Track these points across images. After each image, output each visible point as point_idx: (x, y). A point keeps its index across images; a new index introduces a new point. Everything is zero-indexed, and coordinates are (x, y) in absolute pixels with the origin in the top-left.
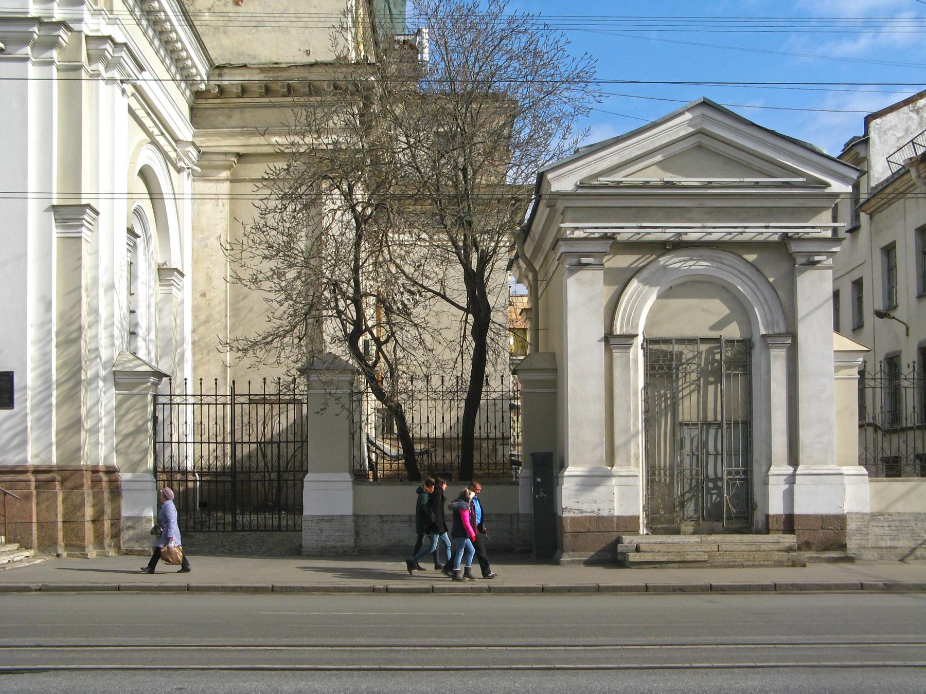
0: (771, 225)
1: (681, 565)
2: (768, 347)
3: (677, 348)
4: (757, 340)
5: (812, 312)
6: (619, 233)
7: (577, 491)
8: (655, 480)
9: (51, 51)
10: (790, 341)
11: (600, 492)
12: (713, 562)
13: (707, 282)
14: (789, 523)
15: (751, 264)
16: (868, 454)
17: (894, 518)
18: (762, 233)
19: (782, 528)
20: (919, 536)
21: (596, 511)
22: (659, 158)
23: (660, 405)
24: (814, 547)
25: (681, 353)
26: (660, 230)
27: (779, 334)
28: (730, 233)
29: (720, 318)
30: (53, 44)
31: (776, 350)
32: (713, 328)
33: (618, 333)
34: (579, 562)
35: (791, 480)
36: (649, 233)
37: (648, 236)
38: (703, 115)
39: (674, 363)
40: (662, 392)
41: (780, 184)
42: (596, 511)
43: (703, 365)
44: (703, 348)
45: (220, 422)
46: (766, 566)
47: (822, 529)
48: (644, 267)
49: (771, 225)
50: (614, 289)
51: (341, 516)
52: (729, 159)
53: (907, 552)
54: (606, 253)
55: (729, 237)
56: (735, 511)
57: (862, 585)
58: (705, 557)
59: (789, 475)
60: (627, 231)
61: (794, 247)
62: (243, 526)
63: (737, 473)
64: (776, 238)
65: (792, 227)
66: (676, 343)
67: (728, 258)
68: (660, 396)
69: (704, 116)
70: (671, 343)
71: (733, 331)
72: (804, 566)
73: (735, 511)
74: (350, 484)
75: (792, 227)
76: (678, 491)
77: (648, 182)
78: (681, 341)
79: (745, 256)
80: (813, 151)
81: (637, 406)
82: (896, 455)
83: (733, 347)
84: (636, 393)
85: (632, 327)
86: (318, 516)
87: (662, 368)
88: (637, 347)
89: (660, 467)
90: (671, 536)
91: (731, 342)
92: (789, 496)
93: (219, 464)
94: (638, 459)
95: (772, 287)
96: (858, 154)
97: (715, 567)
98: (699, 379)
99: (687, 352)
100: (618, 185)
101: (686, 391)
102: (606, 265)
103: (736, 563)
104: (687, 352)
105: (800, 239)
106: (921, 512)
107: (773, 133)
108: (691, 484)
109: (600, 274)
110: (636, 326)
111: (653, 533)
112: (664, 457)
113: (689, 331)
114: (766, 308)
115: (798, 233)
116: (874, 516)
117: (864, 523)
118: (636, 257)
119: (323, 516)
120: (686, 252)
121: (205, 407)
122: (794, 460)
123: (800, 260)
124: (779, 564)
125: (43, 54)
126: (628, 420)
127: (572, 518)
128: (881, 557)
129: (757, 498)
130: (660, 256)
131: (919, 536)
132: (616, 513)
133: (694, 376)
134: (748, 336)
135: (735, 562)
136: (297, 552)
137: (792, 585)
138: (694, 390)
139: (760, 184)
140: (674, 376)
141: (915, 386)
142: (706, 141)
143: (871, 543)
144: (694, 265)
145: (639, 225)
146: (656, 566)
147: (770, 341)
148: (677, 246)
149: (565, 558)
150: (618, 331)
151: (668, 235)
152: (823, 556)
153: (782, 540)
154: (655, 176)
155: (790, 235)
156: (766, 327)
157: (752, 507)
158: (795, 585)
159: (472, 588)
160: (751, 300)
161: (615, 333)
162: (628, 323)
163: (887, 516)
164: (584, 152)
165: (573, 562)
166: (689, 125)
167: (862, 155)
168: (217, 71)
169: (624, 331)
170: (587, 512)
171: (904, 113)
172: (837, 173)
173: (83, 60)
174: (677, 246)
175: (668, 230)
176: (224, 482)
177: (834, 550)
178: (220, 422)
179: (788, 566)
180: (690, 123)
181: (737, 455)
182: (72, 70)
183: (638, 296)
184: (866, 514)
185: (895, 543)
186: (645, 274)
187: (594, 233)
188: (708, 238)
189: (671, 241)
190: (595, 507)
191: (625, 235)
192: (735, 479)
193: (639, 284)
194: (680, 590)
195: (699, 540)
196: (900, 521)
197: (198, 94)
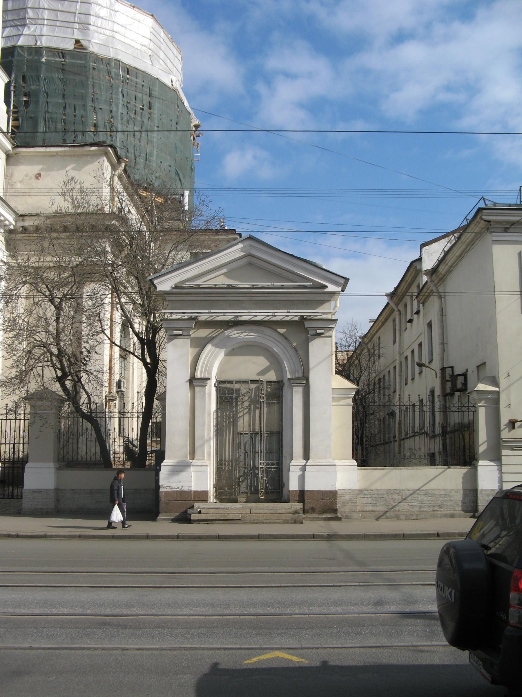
0: (291, 311)
1: (224, 522)
2: (291, 386)
3: (237, 386)
4: (286, 381)
5: (318, 364)
6: (200, 316)
7: (168, 475)
8: (222, 468)
10: (305, 382)
11: (183, 476)
12: (245, 520)
13: (256, 346)
14: (302, 495)
15: (282, 335)
16: (421, 452)
17: (375, 492)
18: (288, 316)
19: (298, 499)
20: (389, 504)
21: (180, 487)
22: (224, 271)
23: (226, 422)
24: (317, 511)
25: (239, 390)
26: (222, 314)
27: (299, 378)
28: (268, 316)
29: (264, 368)
31: (297, 388)
32: (258, 374)
33: (199, 377)
34: (168, 519)
35: (304, 468)
36: (218, 316)
37: (218, 318)
38: (250, 245)
39: (234, 396)
40: (228, 413)
41: (297, 286)
42: (180, 487)
43: (253, 397)
44: (253, 386)
45: (17, 430)
46: (278, 523)
47: (322, 499)
48: (216, 336)
49: (291, 311)
50: (197, 350)
51: (47, 489)
52: (268, 271)
53: (382, 513)
54: (191, 328)
55: (268, 318)
56: (270, 488)
57: (313, 535)
58: (240, 517)
59: (303, 466)
60: (204, 315)
61: (307, 325)
62: (17, 496)
63: (273, 464)
64: (296, 319)
65: (306, 312)
66: (236, 383)
67: (268, 331)
68: (226, 416)
69: (251, 246)
70: (233, 383)
71: (272, 376)
72: (302, 523)
73: (270, 488)
74: (53, 470)
75: (306, 312)
76: (235, 474)
77: (216, 285)
78: (238, 382)
79: (279, 330)
80: (316, 266)
81: (210, 422)
82: (433, 452)
83: (271, 385)
84: (209, 414)
85: (208, 373)
86: (32, 490)
87: (226, 399)
88: (211, 386)
89: (225, 460)
90: (224, 504)
91: (270, 382)
92: (302, 479)
93: (15, 456)
94: (210, 455)
95: (295, 349)
96: (416, 267)
97: (246, 523)
98: (250, 405)
99: (244, 388)
100: (199, 287)
101: (241, 414)
102: (192, 336)
103: (259, 521)
104: (244, 388)
105: (311, 320)
106: (391, 488)
107: (291, 255)
108: (244, 471)
109: (188, 341)
110: (210, 373)
111: (220, 502)
112: (228, 455)
113: (244, 376)
114: (291, 362)
115: (310, 316)
116: (361, 491)
117: (354, 496)
118: (211, 330)
119: (36, 490)
120: (241, 327)
121: (8, 421)
122: (306, 456)
123: (312, 332)
124: (286, 522)
126: (204, 431)
127: (165, 492)
128: (364, 517)
129: (285, 480)
130: (225, 330)
131: (389, 504)
132: (193, 489)
133: (246, 404)
134: (280, 379)
135: (259, 520)
136: (19, 513)
137: (269, 535)
138: (246, 413)
139: (285, 286)
140: (234, 404)
141: (430, 410)
142: (254, 260)
143: (358, 508)
144: (247, 335)
145: (209, 311)
146: (208, 522)
147: (292, 382)
148: (236, 324)
149: (160, 517)
150: (198, 375)
151: (229, 317)
152: (321, 516)
153: (294, 507)
154: (222, 281)
155: (305, 317)
156: (291, 373)
157: (281, 485)
158: (272, 535)
159: (69, 535)
160: (282, 357)
161: (196, 377)
162: (205, 371)
163: (370, 491)
164: (175, 267)
165: (164, 519)
166: (242, 251)
167: (418, 268)
168: (21, 218)
169: (203, 376)
170: (175, 488)
171: (442, 243)
172: (331, 279)
174: (236, 324)
175: (227, 314)
176: (18, 467)
177: (330, 513)
178: (17, 430)
179: (292, 523)
180: (242, 250)
181: (272, 452)
183: (212, 354)
184: (356, 490)
185: (375, 508)
186: (216, 341)
187: (184, 316)
188: (274, 319)
189: (232, 321)
190: (179, 485)
192: (271, 468)
193: (213, 347)
194: (199, 538)
195: (241, 506)
196: (378, 494)
197: (11, 232)
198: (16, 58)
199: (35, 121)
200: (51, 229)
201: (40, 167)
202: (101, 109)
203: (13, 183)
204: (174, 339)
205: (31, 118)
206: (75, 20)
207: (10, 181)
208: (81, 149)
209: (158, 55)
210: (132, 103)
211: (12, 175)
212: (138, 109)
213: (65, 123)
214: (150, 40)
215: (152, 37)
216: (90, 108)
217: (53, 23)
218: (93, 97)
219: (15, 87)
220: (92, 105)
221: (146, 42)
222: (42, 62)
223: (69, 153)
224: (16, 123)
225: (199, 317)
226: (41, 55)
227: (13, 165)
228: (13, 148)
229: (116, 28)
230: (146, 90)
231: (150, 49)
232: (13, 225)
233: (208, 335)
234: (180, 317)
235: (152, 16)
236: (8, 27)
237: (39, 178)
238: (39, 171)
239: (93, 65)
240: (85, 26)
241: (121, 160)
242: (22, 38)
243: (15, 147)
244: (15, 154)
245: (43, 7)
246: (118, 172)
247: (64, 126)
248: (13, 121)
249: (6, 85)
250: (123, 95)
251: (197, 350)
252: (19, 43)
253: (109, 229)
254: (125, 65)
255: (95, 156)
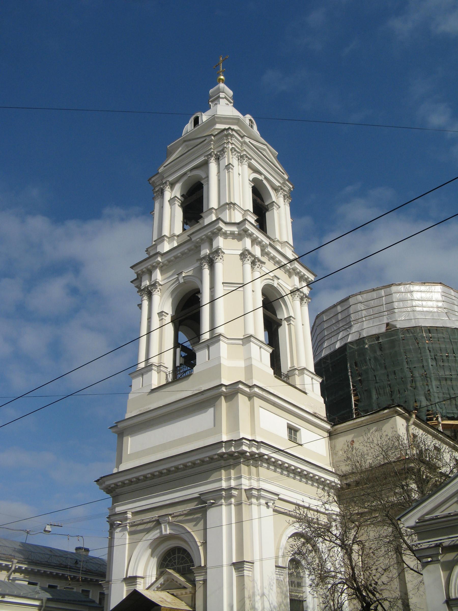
6: (444, 542)
9: (231, 500)
30: (231, 496)
50: (448, 573)
100: (437, 518)
102: (441, 561)
109: (439, 566)
125: (228, 501)
145: (448, 537)
168: (344, 478)
173: (163, 526)
182: (239, 504)
187: (432, 544)
191: (447, 542)
198: (348, 351)
199: (369, 392)
200: (368, 480)
201: (353, 435)
202: (415, 367)
203: (336, 452)
204: (426, 566)
205: (366, 390)
206: (384, 310)
207: (334, 451)
208: (377, 414)
209: (453, 310)
210: (438, 354)
211: (335, 446)
212: (445, 358)
213: (390, 387)
214: (443, 301)
215: (444, 299)
216: (407, 369)
217: (371, 317)
218: (407, 361)
219: (351, 372)
220: (408, 367)
221: (440, 304)
222: (367, 348)
223: (370, 420)
224: (357, 397)
225: (443, 543)
226: (364, 343)
227: (334, 439)
228: (332, 427)
229: (414, 303)
230: (447, 340)
231: (445, 308)
232: (339, 484)
233: (455, 557)
234: (428, 545)
235: (440, 283)
236: (341, 332)
237: (353, 443)
238: (352, 438)
239: (402, 337)
240: (391, 311)
241: (411, 413)
242: (350, 337)
243: (333, 426)
244: (335, 430)
245: (361, 310)
246: (411, 422)
247: (390, 389)
248: (354, 397)
249: (321, 384)
250: (430, 351)
251: (448, 573)
252: (349, 340)
253: (410, 470)
254: (426, 328)
255: (389, 417)
